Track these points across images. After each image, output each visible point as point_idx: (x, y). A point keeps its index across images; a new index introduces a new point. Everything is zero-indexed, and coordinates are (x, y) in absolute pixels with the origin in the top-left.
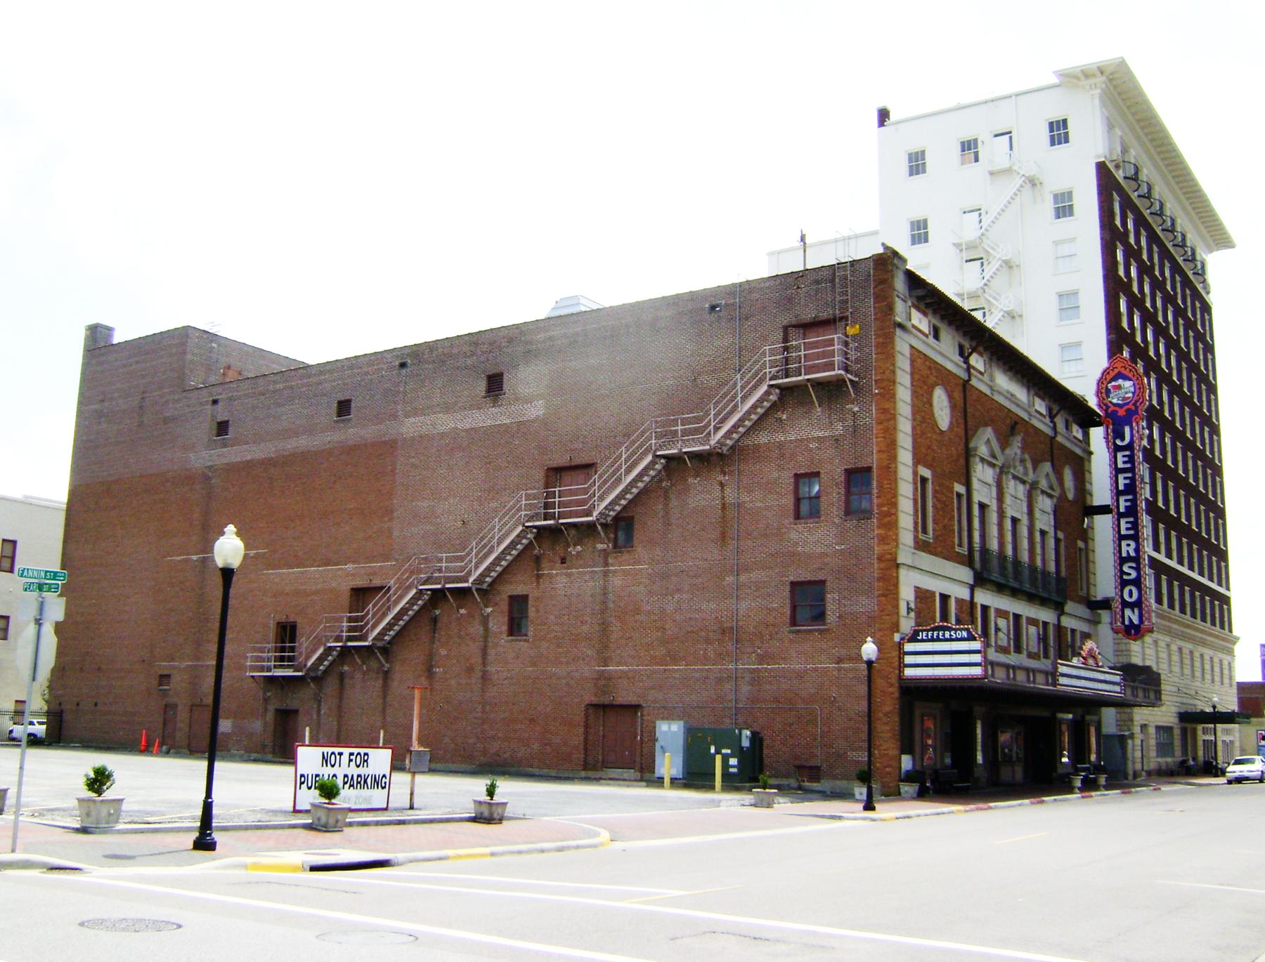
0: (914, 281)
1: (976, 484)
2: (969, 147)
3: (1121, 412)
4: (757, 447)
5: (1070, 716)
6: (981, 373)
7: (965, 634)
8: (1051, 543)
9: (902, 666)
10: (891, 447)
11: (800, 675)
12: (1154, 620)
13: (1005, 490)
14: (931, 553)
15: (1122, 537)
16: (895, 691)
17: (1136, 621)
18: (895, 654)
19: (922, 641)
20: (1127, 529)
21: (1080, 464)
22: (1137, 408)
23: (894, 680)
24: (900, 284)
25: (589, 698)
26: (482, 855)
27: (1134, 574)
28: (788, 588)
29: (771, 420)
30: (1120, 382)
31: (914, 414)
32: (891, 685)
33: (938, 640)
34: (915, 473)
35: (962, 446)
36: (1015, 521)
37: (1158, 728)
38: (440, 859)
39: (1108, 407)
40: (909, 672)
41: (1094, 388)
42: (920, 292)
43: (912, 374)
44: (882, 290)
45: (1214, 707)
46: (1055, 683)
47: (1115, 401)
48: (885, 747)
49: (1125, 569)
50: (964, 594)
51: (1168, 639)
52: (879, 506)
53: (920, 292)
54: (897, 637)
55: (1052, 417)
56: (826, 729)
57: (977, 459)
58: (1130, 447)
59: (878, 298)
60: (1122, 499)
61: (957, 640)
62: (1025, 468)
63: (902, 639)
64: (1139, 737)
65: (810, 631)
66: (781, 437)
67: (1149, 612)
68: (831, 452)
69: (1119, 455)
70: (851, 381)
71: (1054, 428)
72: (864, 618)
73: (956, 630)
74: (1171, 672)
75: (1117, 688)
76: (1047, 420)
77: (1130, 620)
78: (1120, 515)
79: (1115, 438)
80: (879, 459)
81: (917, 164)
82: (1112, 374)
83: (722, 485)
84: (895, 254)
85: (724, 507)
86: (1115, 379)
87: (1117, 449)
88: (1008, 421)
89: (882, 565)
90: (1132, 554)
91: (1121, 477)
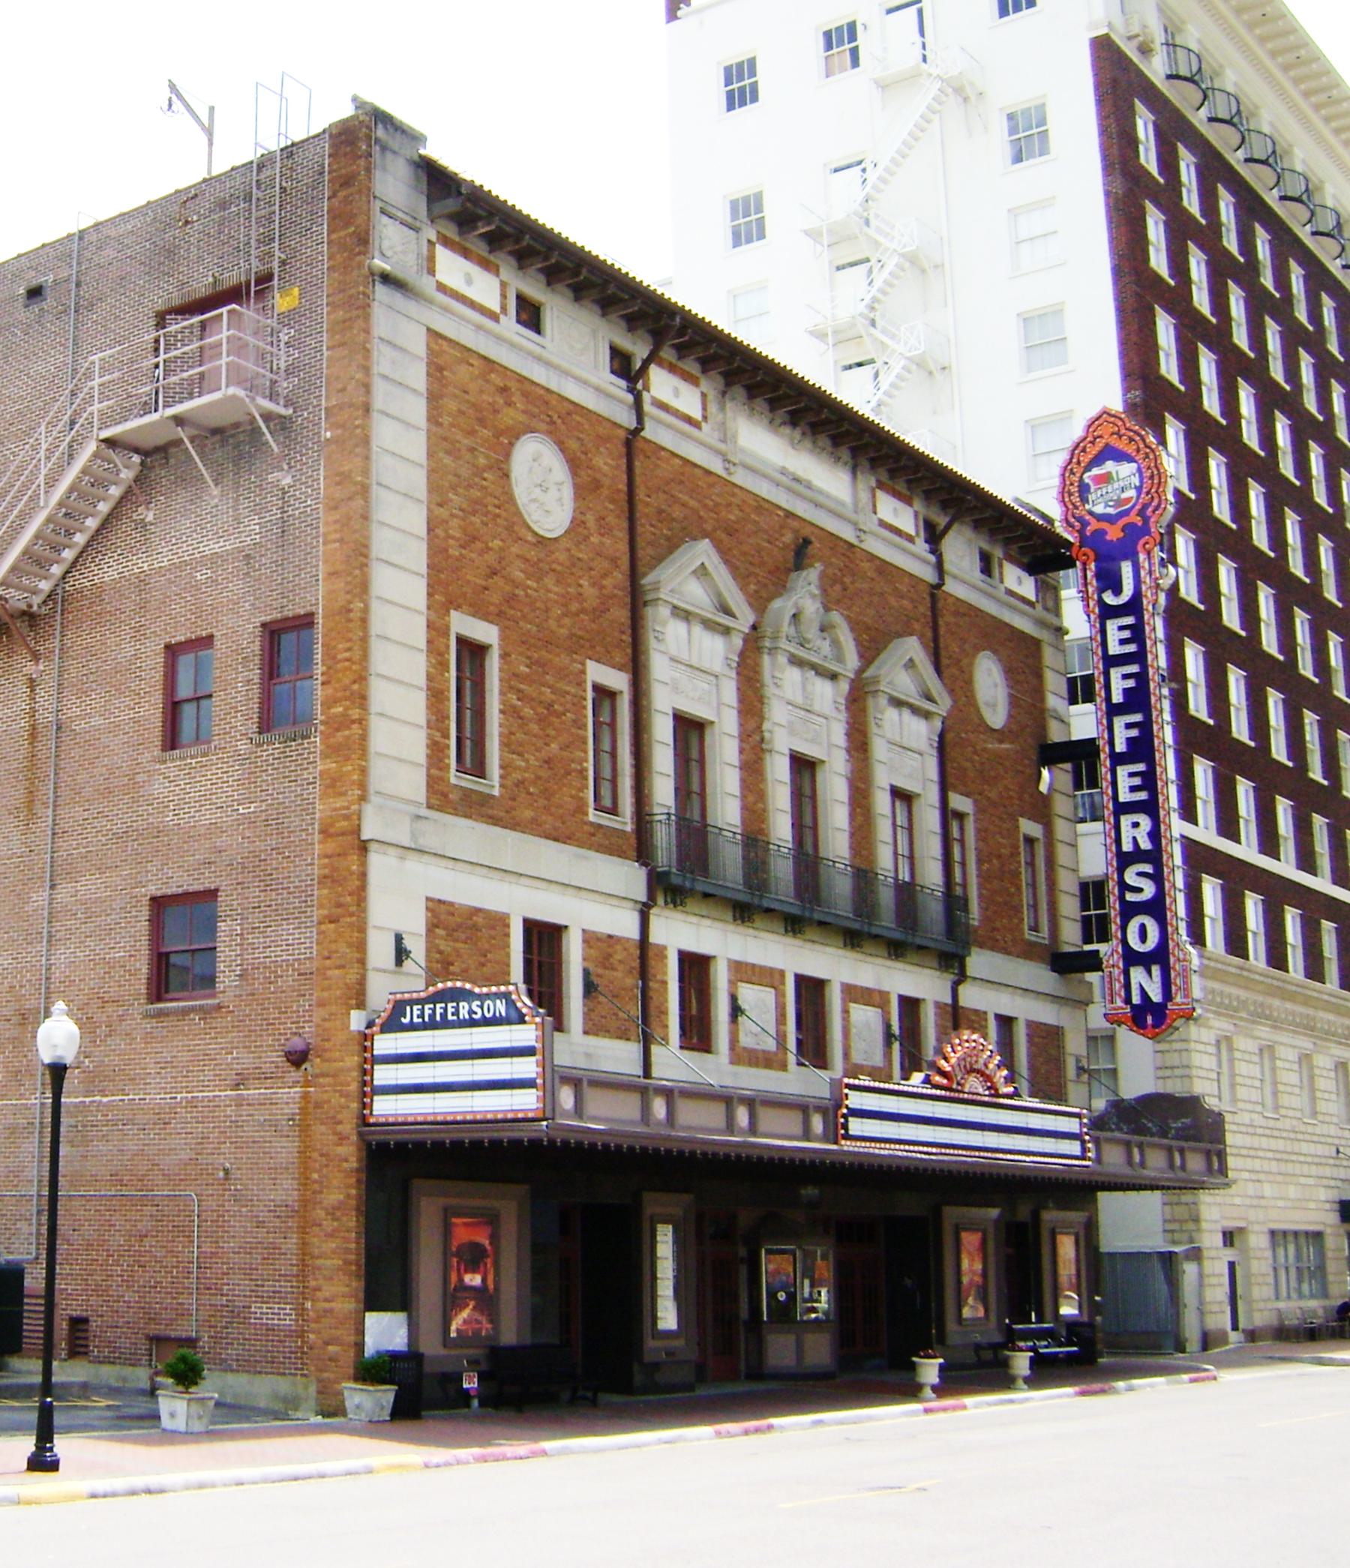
0: (437, 181)
1: (659, 667)
2: (842, 41)
3: (1114, 533)
4: (99, 590)
5: (994, 1213)
7: (501, 1007)
8: (929, 818)
9: (368, 1090)
10: (356, 563)
11: (163, 1119)
12: (1196, 993)
13: (770, 690)
14: (495, 821)
15: (1122, 809)
16: (349, 1154)
17: (1156, 996)
19: (412, 1027)
20: (1133, 789)
21: (1024, 658)
22: (1146, 520)
23: (349, 1127)
24: (393, 183)
26: (73, 1498)
27: (1149, 890)
28: (145, 913)
29: (125, 526)
30: (1109, 466)
31: (433, 488)
32: (342, 1138)
33: (445, 1024)
34: (436, 630)
35: (619, 577)
36: (803, 766)
37: (1276, 1237)
38: (201, 1486)
39: (1084, 524)
40: (384, 1107)
42: (451, 205)
43: (433, 398)
44: (347, 201)
46: (836, 1130)
47: (1099, 509)
48: (326, 1293)
49: (1130, 877)
50: (624, 924)
51: (1306, 1044)
52: (328, 704)
53: (451, 205)
54: (357, 1020)
55: (934, 536)
56: (207, 1248)
57: (883, 701)
58: (1134, 606)
59: (340, 218)
60: (1119, 722)
61: (486, 1022)
62: (836, 644)
63: (370, 1025)
64: (1216, 1265)
65: (185, 1012)
66: (141, 564)
67: (1185, 973)
68: (237, 587)
69: (1112, 626)
70: (268, 417)
71: (939, 567)
72: (289, 980)
73: (482, 997)
74: (1314, 1114)
75: (1074, 1147)
76: (921, 547)
77: (1143, 993)
79: (1101, 591)
80: (330, 594)
81: (740, 87)
82: (1093, 451)
83: (32, 684)
84: (381, 117)
85: (33, 734)
86: (1098, 460)
87: (1108, 612)
88: (788, 538)
89: (331, 846)
90: (1145, 844)
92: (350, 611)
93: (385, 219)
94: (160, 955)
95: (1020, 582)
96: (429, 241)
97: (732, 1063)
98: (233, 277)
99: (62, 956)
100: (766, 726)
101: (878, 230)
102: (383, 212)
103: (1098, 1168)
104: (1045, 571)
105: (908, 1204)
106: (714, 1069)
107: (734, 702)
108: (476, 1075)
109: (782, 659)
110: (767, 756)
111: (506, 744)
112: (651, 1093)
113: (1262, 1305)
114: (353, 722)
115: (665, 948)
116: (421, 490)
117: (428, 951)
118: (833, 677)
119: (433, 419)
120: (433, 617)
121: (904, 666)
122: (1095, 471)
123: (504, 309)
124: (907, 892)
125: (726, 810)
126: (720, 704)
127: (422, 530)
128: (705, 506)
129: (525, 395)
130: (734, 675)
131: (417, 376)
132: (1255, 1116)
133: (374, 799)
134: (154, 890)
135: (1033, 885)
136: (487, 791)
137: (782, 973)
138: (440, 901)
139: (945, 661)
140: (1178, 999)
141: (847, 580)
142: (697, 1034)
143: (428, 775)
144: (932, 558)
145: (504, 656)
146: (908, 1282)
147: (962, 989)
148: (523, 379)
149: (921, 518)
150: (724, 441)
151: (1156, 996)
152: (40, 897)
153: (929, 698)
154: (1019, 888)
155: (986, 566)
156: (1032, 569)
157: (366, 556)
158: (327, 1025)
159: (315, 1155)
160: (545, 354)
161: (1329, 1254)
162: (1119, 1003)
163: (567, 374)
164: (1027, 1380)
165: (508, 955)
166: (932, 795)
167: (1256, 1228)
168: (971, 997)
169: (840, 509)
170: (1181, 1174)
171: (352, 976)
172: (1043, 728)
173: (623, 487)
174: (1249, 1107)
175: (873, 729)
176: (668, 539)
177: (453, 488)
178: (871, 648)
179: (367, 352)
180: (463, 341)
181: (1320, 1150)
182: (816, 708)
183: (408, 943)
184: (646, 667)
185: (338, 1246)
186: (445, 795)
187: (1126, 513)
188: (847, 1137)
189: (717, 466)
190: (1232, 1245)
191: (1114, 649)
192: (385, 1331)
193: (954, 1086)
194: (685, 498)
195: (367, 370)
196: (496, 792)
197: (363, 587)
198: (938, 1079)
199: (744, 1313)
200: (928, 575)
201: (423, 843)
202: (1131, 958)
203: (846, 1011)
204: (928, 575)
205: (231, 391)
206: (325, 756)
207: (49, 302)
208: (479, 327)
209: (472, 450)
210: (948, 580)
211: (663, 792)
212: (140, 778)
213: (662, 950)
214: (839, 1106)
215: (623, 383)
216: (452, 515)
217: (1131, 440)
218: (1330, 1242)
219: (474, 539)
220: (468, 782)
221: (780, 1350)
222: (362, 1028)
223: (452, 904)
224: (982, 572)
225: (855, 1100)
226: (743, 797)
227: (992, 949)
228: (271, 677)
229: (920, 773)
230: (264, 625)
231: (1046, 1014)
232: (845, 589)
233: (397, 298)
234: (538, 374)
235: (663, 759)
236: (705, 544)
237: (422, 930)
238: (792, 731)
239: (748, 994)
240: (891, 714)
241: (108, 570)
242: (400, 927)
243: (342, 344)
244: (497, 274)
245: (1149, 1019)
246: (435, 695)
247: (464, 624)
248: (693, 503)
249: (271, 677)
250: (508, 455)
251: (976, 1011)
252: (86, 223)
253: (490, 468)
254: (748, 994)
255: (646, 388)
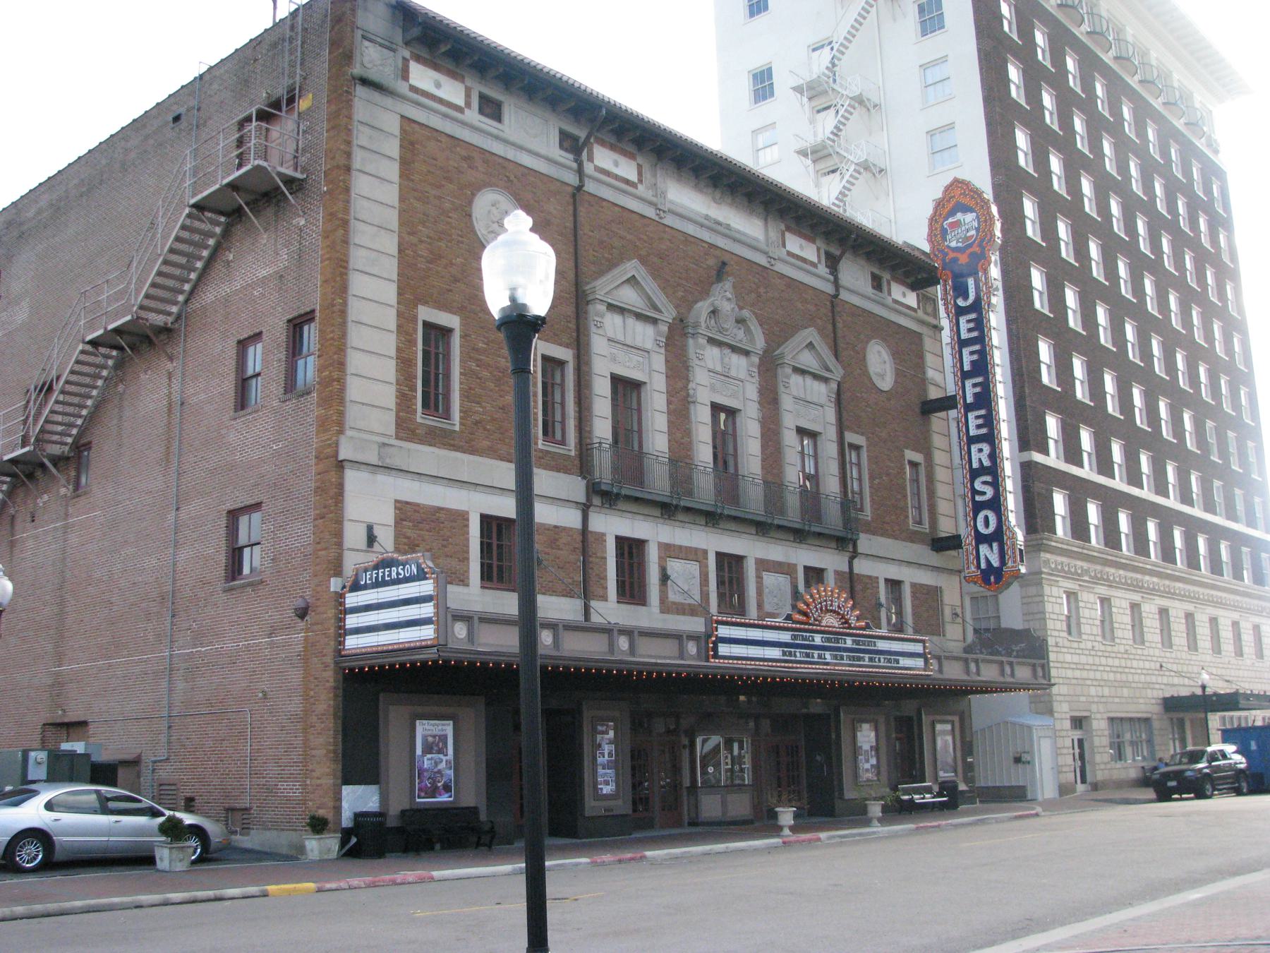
1: (598, 345)
3: (963, 259)
6: (814, 265)
8: (830, 449)
9: (342, 632)
13: (694, 362)
15: (972, 440)
17: (996, 563)
18: (331, 613)
25: (46, 716)
27: (990, 492)
30: (959, 216)
36: (625, 388)
40: (352, 642)
41: (925, 230)
45: (1204, 687)
47: (953, 244)
49: (978, 486)
53: (416, 31)
55: (833, 263)
57: (789, 370)
60: (969, 383)
63: (344, 587)
66: (226, 289)
69: (962, 320)
71: (836, 283)
75: (920, 663)
76: (823, 270)
77: (991, 547)
78: (969, 408)
79: (956, 298)
80: (324, 294)
86: (952, 213)
87: (960, 311)
88: (711, 262)
90: (986, 463)
91: (965, 351)
92: (333, 305)
93: (366, 43)
94: (234, 550)
95: (904, 295)
96: (404, 58)
97: (662, 612)
98: (281, 92)
99: (184, 555)
100: (691, 385)
101: (841, 86)
102: (364, 37)
103: (940, 676)
104: (922, 288)
105: (817, 706)
106: (649, 616)
107: (662, 368)
108: (394, 620)
109: (702, 341)
110: (692, 407)
111: (466, 395)
112: (616, 633)
113: (1102, 766)
114: (334, 380)
115: (603, 535)
116: (394, 223)
117: (396, 537)
118: (747, 353)
119: (403, 175)
120: (402, 308)
121: (807, 348)
122: (950, 220)
123: (468, 104)
124: (812, 498)
125: (657, 441)
126: (651, 371)
127: (394, 250)
128: (640, 239)
129: (485, 162)
130: (663, 351)
131: (393, 148)
132: (1096, 644)
133: (349, 433)
134: (230, 506)
135: (918, 494)
136: (449, 427)
137: (705, 552)
138: (407, 503)
139: (841, 345)
140: (1010, 564)
141: (762, 290)
142: (632, 590)
143: (398, 417)
144: (832, 278)
145: (464, 336)
146: (818, 758)
147: (856, 562)
148: (483, 151)
149: (822, 252)
150: (656, 196)
151: (996, 563)
152: (171, 516)
153: (828, 369)
154: (905, 496)
155: (877, 283)
156: (913, 287)
157: (346, 268)
158: (319, 589)
159: (312, 679)
160: (501, 134)
161: (1156, 732)
162: (973, 568)
163: (521, 148)
164: (880, 820)
165: (468, 540)
166: (832, 433)
167: (1098, 716)
168: (863, 567)
169: (754, 243)
170: (1009, 679)
171: (332, 554)
172: (925, 391)
173: (570, 224)
174: (1092, 638)
175: (781, 389)
176: (608, 260)
177: (423, 223)
178: (778, 334)
179: (349, 131)
180: (431, 125)
181: (1153, 665)
182: (733, 373)
183: (377, 531)
184: (588, 344)
185: (324, 739)
186: (413, 431)
187: (970, 246)
188: (716, 656)
189: (650, 212)
190: (1081, 728)
191: (964, 335)
192: (359, 799)
193: (812, 621)
194: (622, 233)
195: (349, 143)
196: (457, 428)
197: (343, 289)
198: (798, 617)
199: (687, 782)
200: (830, 289)
201: (388, 462)
202: (980, 539)
203: (759, 578)
204: (830, 289)
205: (256, 162)
206: (319, 405)
207: (183, 123)
208: (445, 116)
209: (440, 198)
210: (842, 291)
211: (602, 429)
212: (224, 431)
213: (601, 537)
214: (710, 636)
215: (571, 156)
216: (421, 241)
217: (973, 197)
218: (1156, 724)
219: (440, 257)
220: (431, 421)
221: (710, 806)
222: (339, 590)
223: (418, 505)
224: (874, 288)
225: (723, 631)
226: (670, 433)
227: (882, 535)
228: (294, 355)
229: (825, 419)
230: (289, 321)
231: (926, 578)
232: (759, 296)
233: (376, 96)
234: (498, 148)
235: (602, 407)
236: (635, 262)
237: (391, 521)
238: (713, 389)
239: (675, 566)
240: (796, 379)
241: (209, 296)
242: (370, 520)
243: (333, 128)
244: (463, 82)
245: (992, 579)
246: (404, 362)
247: (426, 313)
248: (629, 237)
249: (294, 355)
250: (470, 203)
251: (870, 577)
252: (204, 69)
253: (456, 209)
254: (675, 566)
255: (591, 159)
